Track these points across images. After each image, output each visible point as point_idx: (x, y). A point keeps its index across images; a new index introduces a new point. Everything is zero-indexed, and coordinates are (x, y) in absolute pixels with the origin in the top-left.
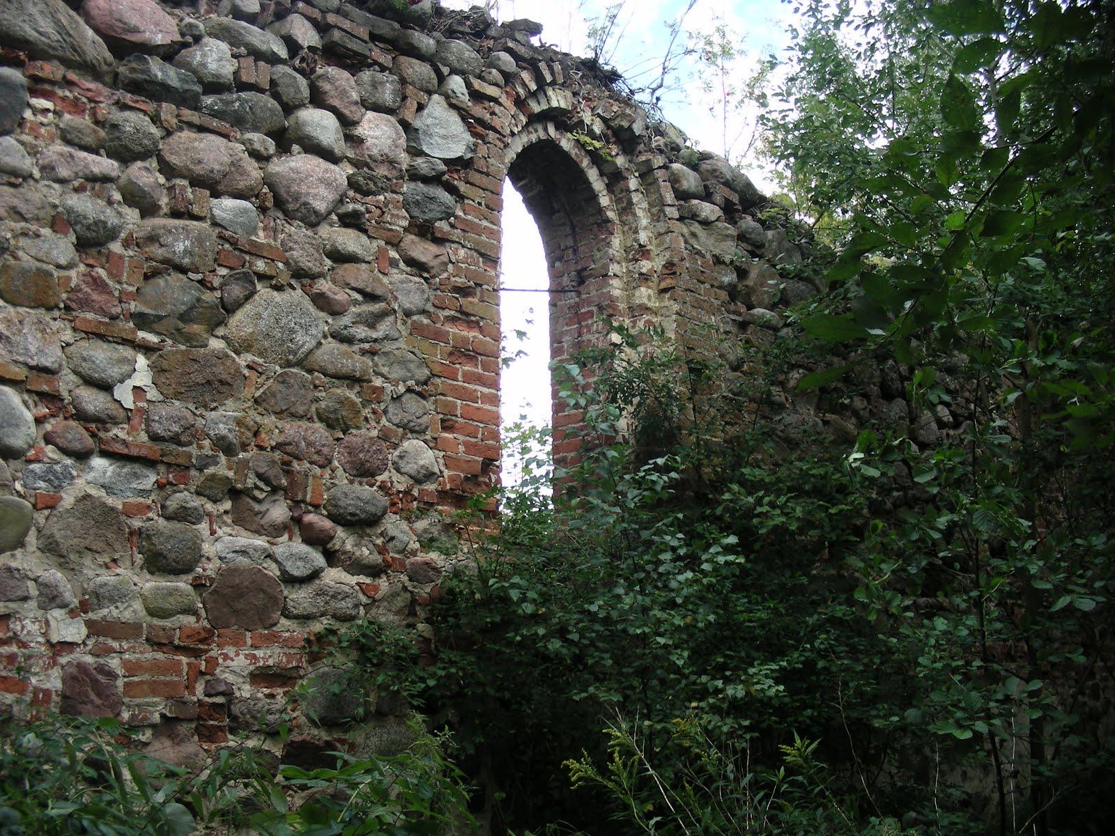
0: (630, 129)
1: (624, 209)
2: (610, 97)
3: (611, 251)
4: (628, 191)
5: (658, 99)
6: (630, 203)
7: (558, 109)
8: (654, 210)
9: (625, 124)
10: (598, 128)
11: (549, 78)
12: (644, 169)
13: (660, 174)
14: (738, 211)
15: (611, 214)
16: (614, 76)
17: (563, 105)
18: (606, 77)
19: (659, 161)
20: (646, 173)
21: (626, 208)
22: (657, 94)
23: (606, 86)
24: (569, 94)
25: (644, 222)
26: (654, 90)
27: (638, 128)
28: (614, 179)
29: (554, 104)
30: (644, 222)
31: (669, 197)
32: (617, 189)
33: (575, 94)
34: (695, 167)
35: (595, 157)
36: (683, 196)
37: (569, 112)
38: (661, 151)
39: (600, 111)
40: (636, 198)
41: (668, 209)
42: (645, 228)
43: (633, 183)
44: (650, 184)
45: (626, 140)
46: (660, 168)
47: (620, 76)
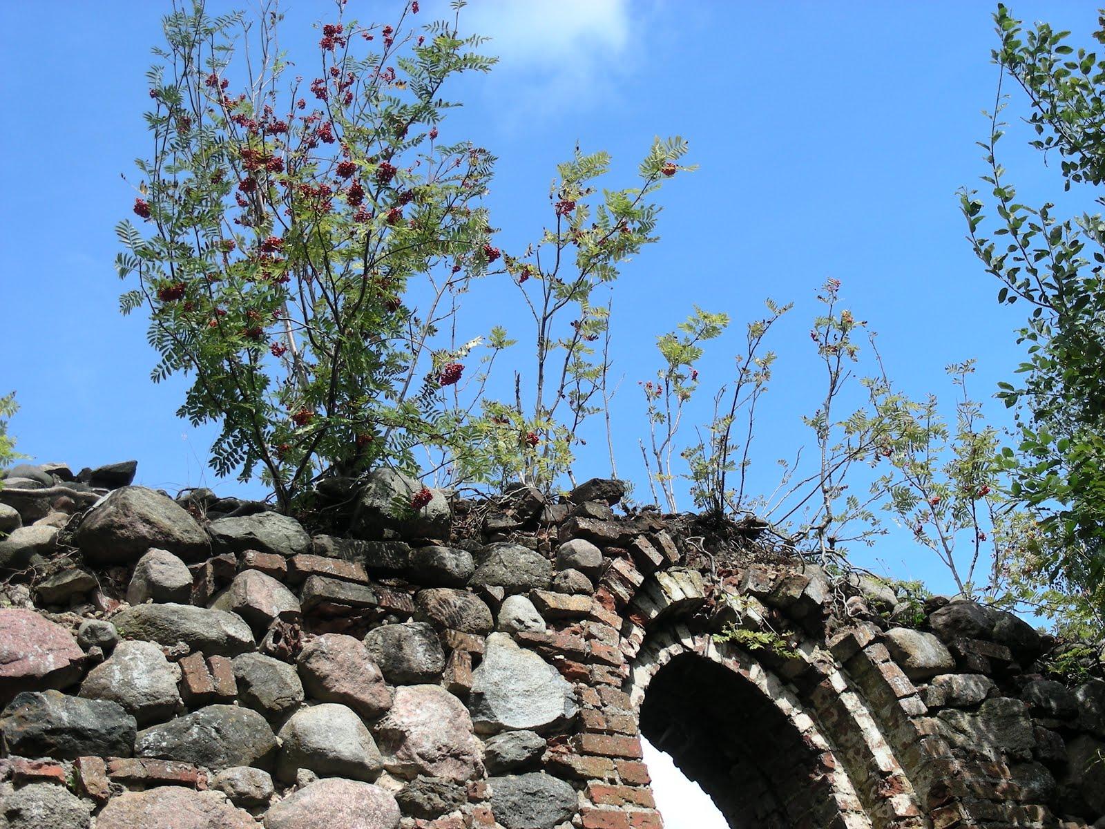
0: (805, 598)
1: (835, 725)
2: (758, 560)
3: (839, 797)
4: (834, 695)
5: (832, 541)
6: (844, 711)
7: (686, 601)
8: (886, 712)
9: (796, 593)
10: (756, 612)
11: (657, 559)
12: (847, 654)
13: (877, 653)
14: (1016, 672)
15: (819, 740)
16: (753, 529)
17: (692, 594)
18: (742, 532)
19: (865, 633)
20: (852, 659)
21: (839, 726)
22: (829, 533)
23: (746, 546)
24: (694, 574)
25: (873, 734)
26: (821, 531)
27: (817, 592)
28: (806, 685)
29: (677, 596)
30: (873, 734)
31: (900, 683)
32: (817, 699)
33: (704, 571)
34: (924, 627)
35: (766, 658)
36: (921, 676)
37: (703, 601)
38: (864, 618)
39: (751, 586)
40: (851, 701)
41: (904, 703)
42: (880, 745)
43: (838, 682)
44: (866, 673)
45: (799, 617)
46: (871, 643)
47: (765, 525)
